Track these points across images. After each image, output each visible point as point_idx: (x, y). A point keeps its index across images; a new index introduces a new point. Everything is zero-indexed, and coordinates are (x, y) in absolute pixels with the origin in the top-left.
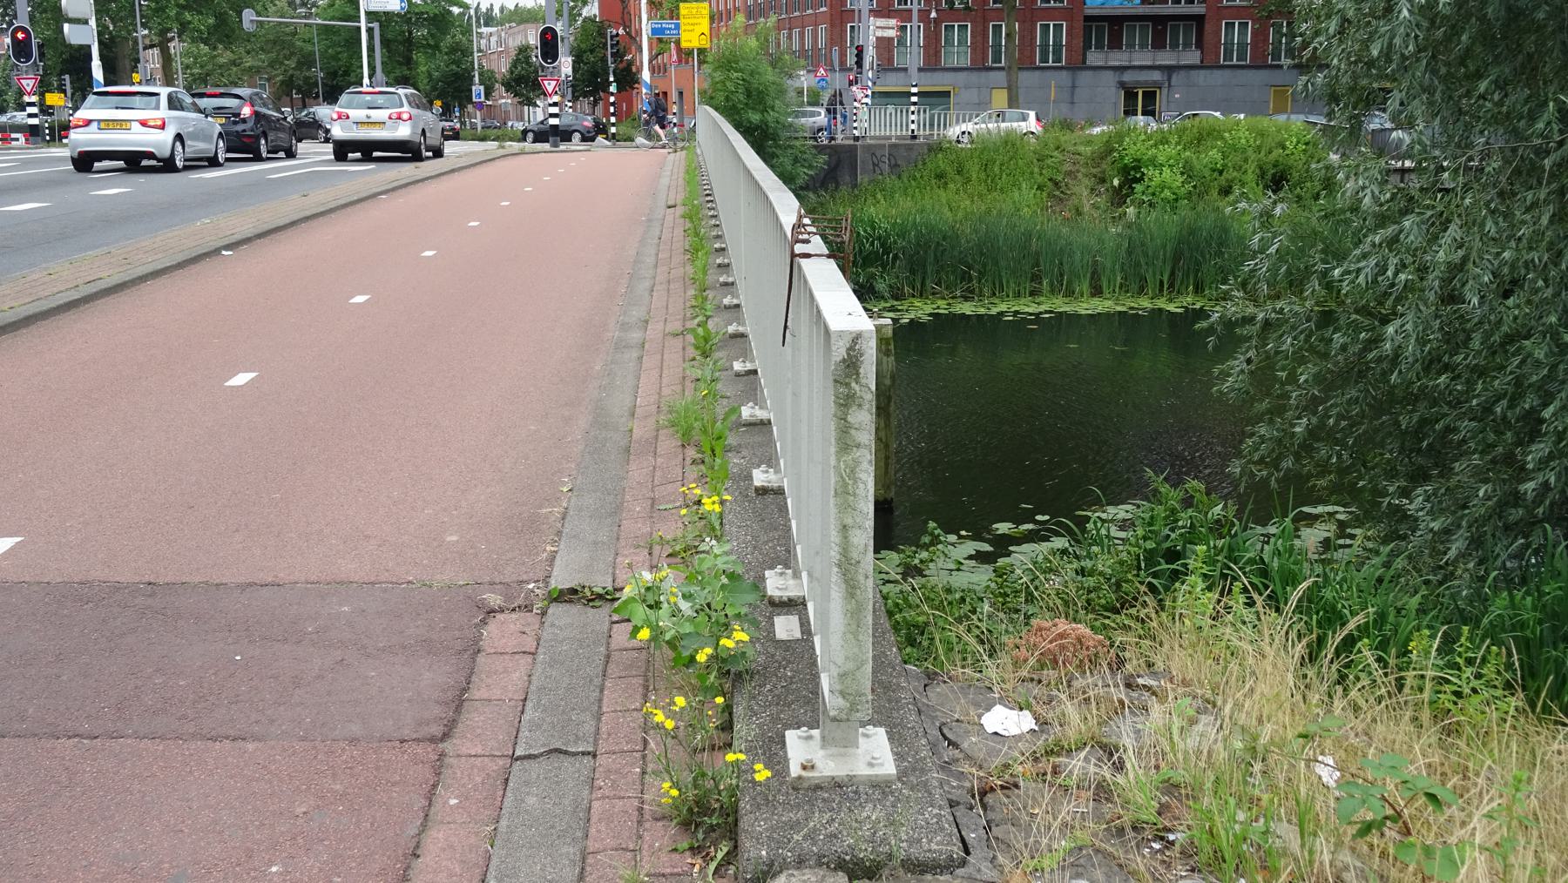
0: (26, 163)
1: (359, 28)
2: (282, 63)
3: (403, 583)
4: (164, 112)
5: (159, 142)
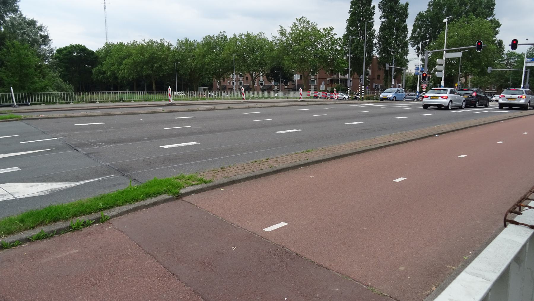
0: (414, 106)
1: (523, 71)
2: (500, 81)
3: (365, 285)
4: (448, 94)
5: (445, 102)
